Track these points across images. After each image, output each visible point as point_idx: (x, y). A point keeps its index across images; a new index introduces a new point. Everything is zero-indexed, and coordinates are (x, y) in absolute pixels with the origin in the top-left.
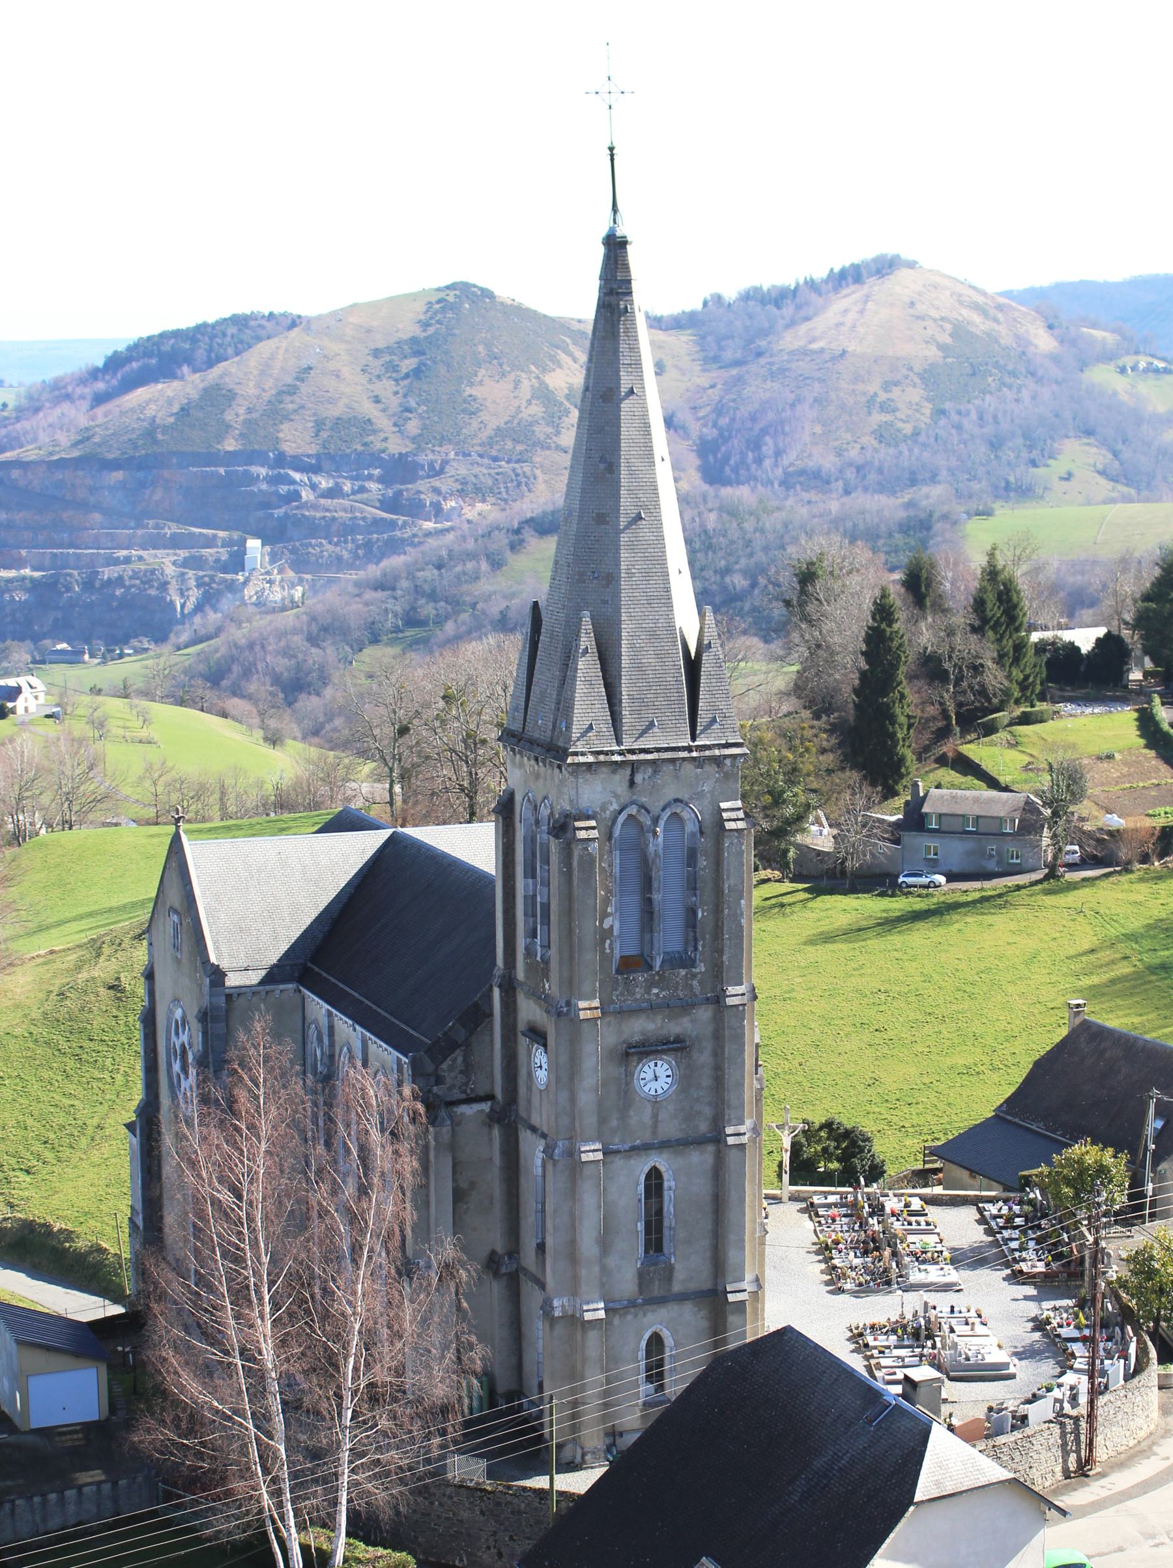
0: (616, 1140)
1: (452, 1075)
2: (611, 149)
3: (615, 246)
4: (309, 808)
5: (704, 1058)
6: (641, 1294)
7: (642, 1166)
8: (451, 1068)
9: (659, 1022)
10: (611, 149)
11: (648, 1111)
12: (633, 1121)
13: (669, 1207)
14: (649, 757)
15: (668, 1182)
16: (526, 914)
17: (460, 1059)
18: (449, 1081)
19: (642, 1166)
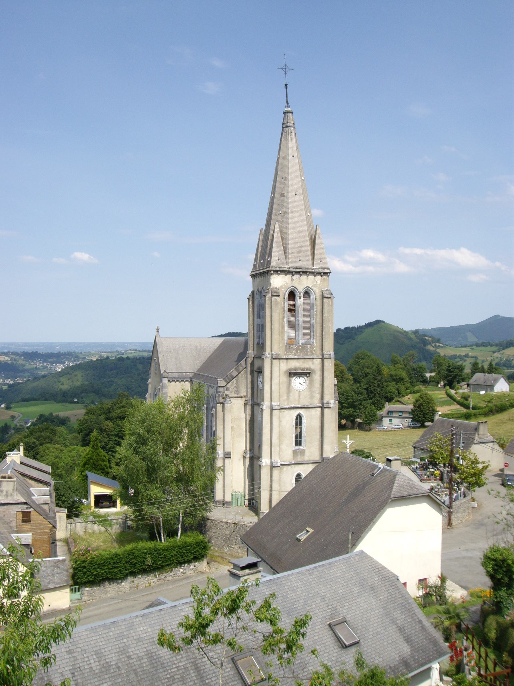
0: (286, 404)
1: (232, 387)
2: (286, 85)
3: (213, 337)
4: (82, 403)
5: (317, 377)
6: (294, 459)
7: (296, 412)
8: (232, 385)
9: (301, 363)
10: (286, 85)
11: (297, 393)
12: (291, 398)
13: (304, 430)
14: (269, 245)
15: (304, 421)
16: (257, 331)
17: (235, 382)
18: (231, 389)
19: (296, 412)
